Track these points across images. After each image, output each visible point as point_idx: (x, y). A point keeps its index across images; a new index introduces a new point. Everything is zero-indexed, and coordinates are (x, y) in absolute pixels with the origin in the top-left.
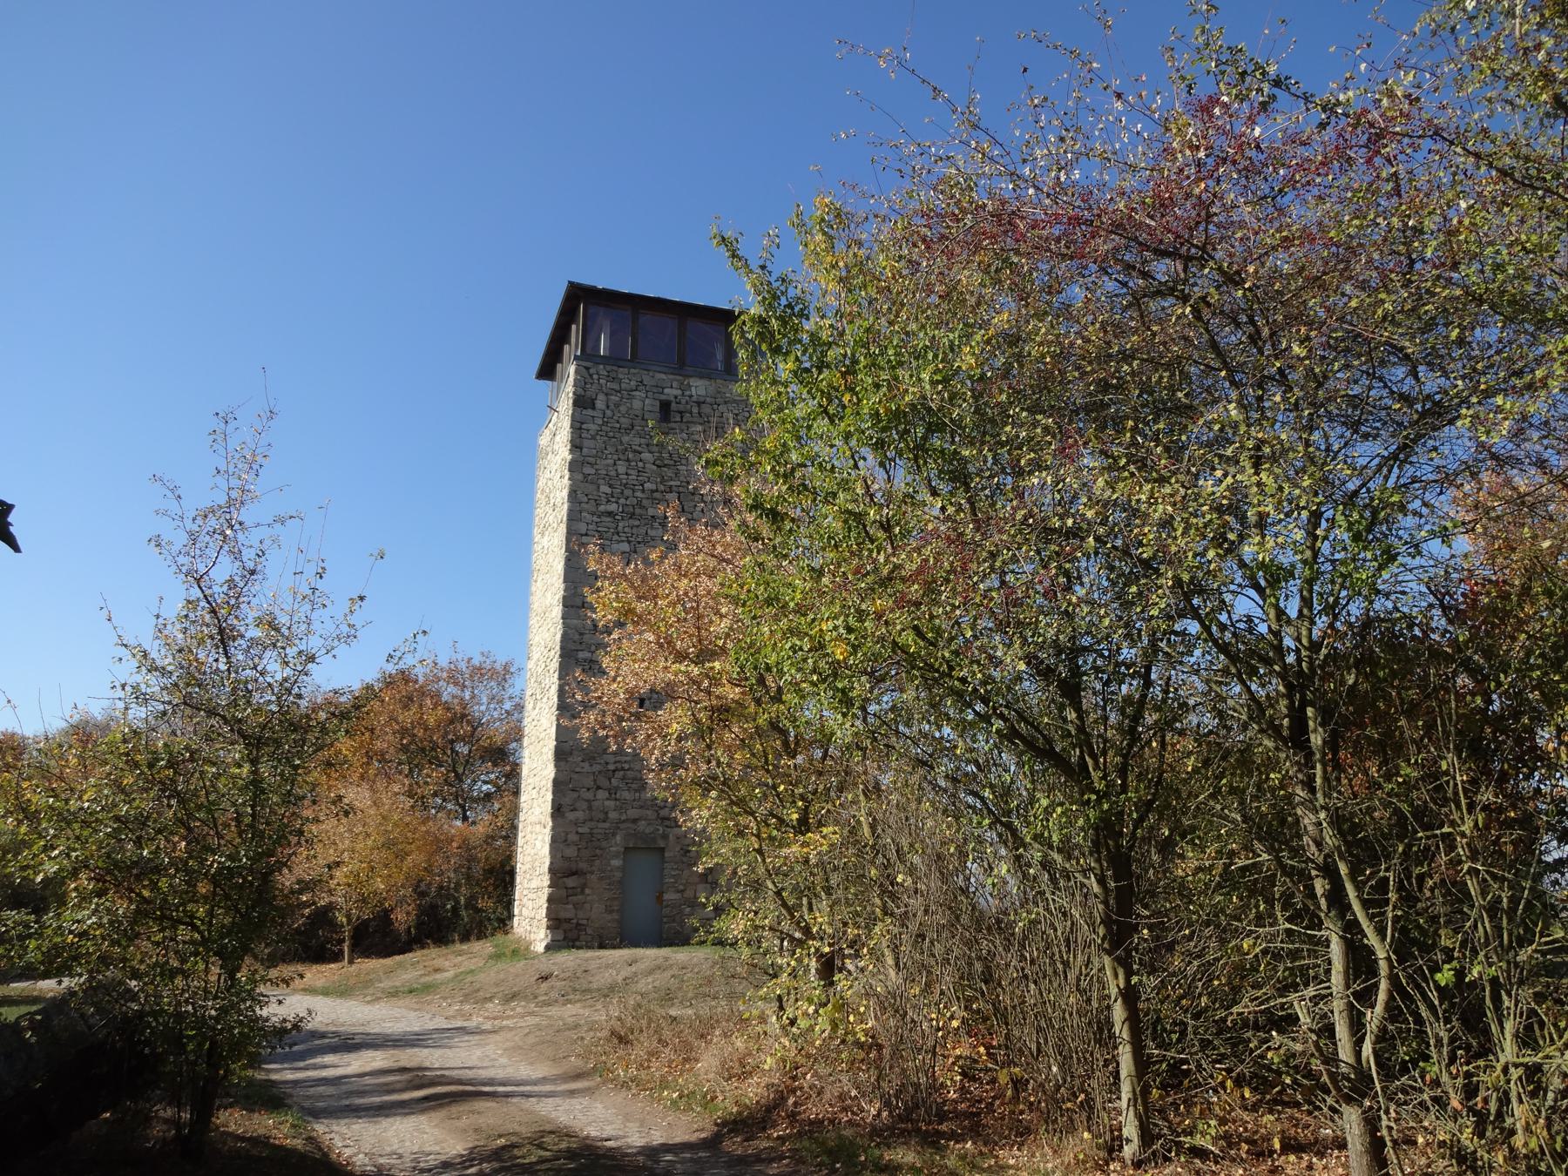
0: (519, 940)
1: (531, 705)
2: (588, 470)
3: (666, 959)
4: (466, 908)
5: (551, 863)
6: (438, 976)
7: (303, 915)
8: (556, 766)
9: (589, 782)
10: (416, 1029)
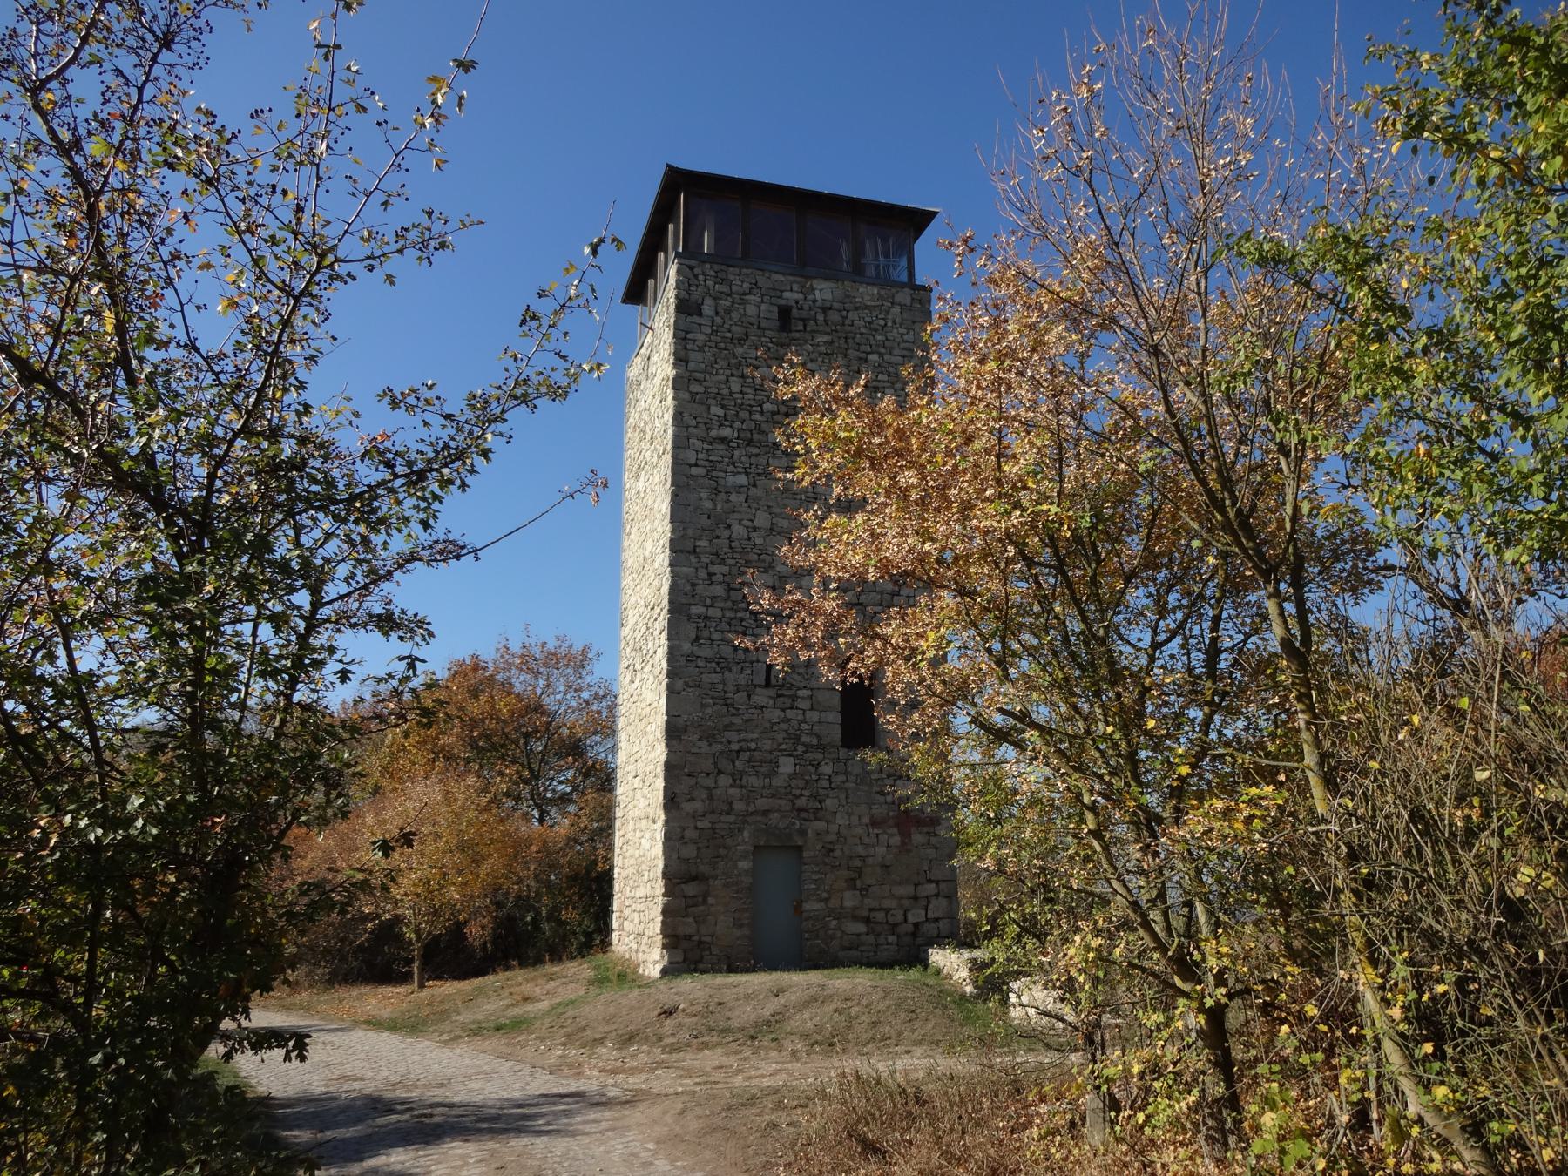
0: (623, 960)
1: (628, 678)
2: (695, 388)
3: (823, 987)
4: (549, 919)
5: (666, 866)
6: (529, 1007)
7: (365, 931)
8: (667, 745)
9: (708, 765)
10: (516, 1094)
